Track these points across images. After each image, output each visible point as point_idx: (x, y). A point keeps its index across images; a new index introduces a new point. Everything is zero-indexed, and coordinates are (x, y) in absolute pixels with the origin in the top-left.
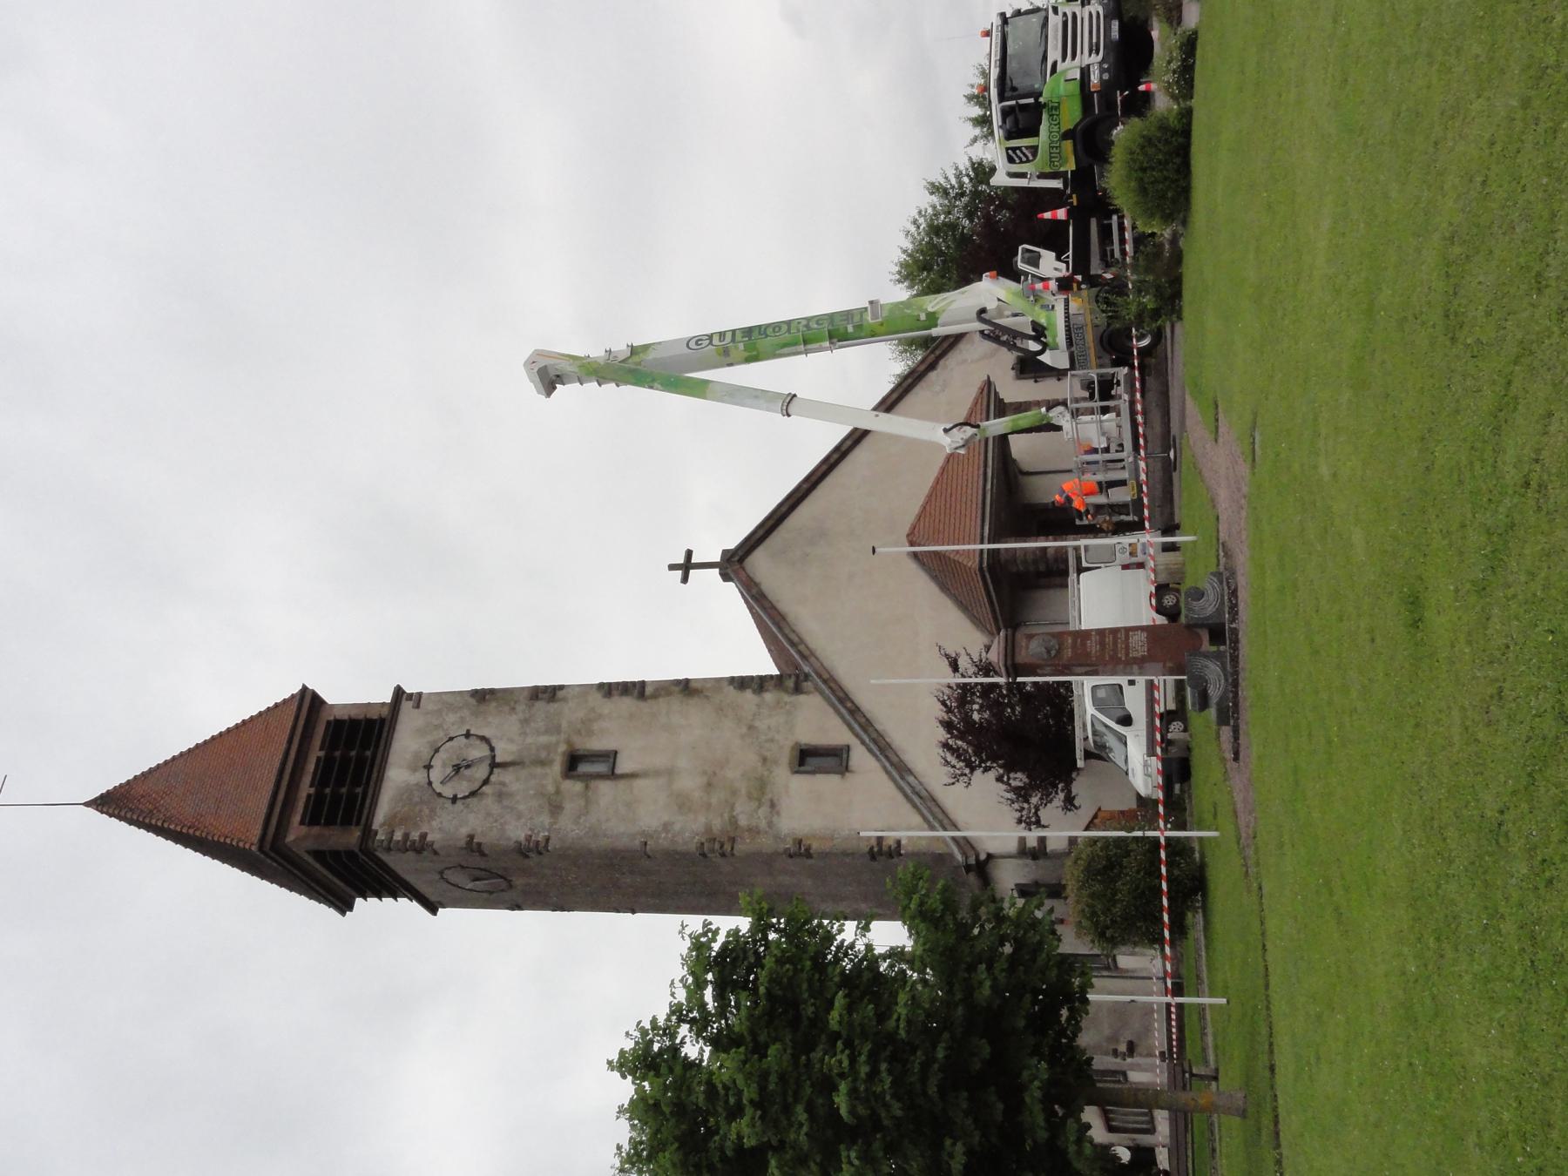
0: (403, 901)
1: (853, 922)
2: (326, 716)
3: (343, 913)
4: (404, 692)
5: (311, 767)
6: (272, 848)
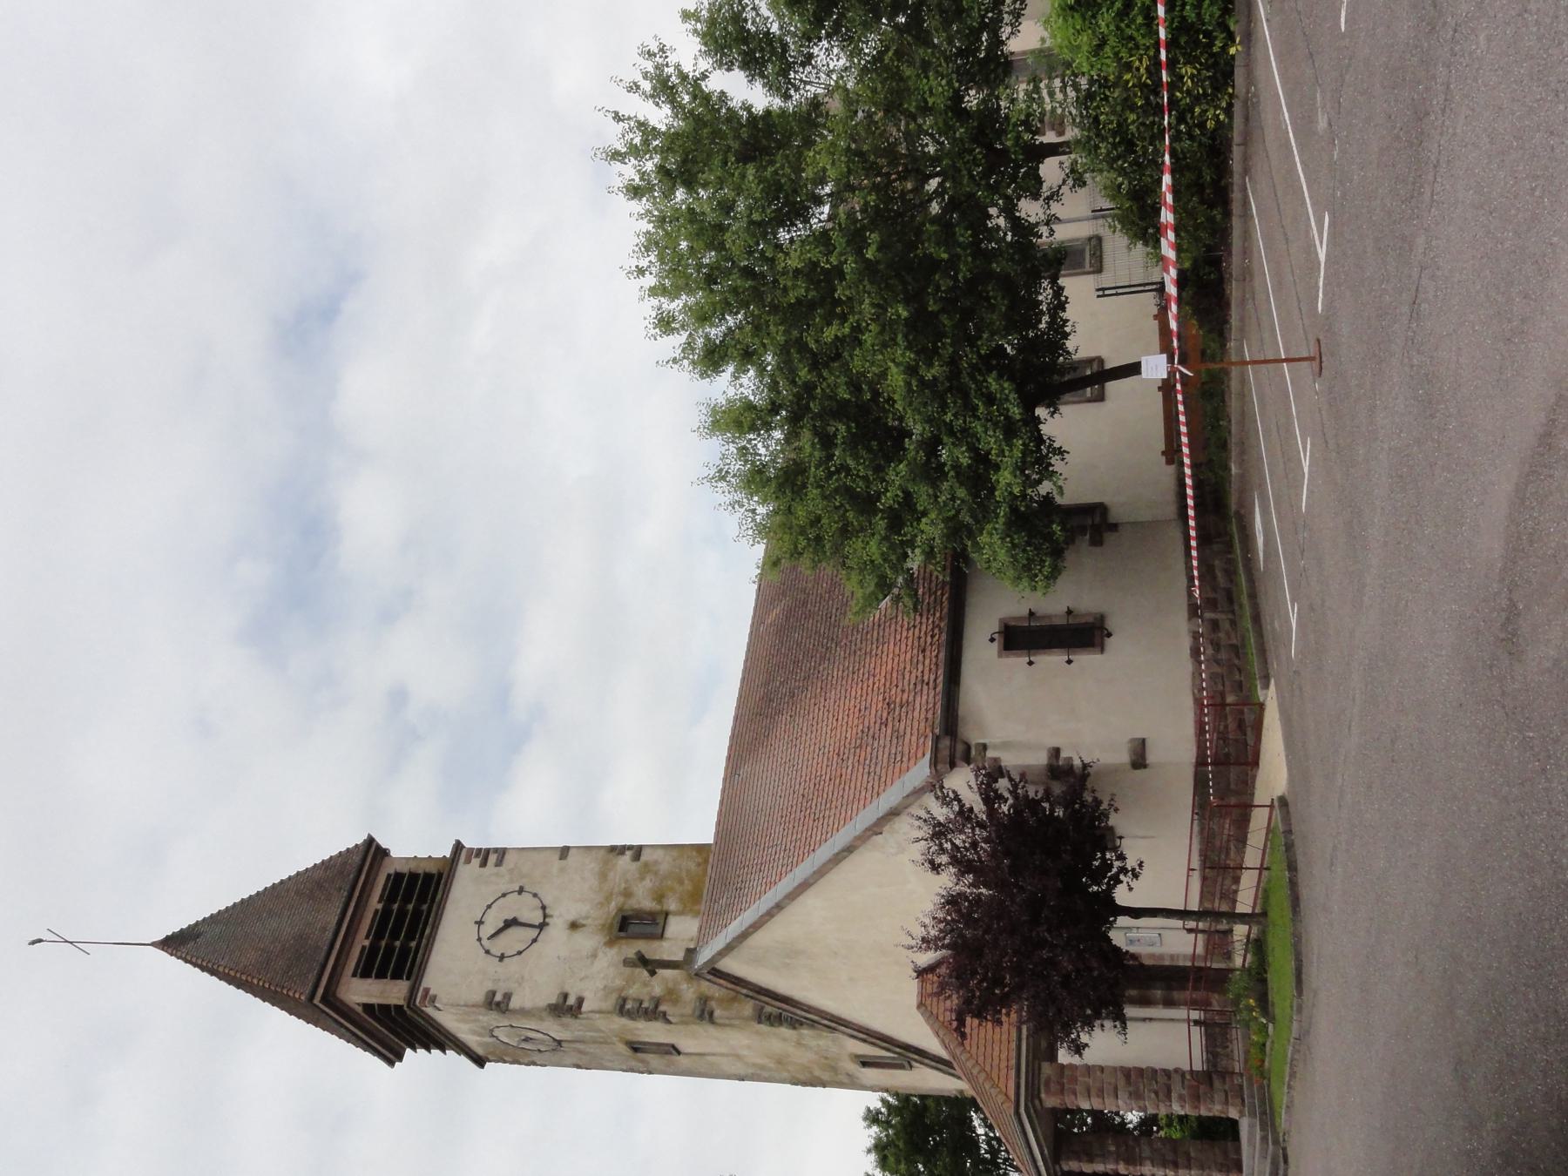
0: (450, 1053)
1: (1111, 366)
2: (388, 869)
3: (391, 1063)
4: (463, 847)
5: (356, 953)
6: (324, 999)
